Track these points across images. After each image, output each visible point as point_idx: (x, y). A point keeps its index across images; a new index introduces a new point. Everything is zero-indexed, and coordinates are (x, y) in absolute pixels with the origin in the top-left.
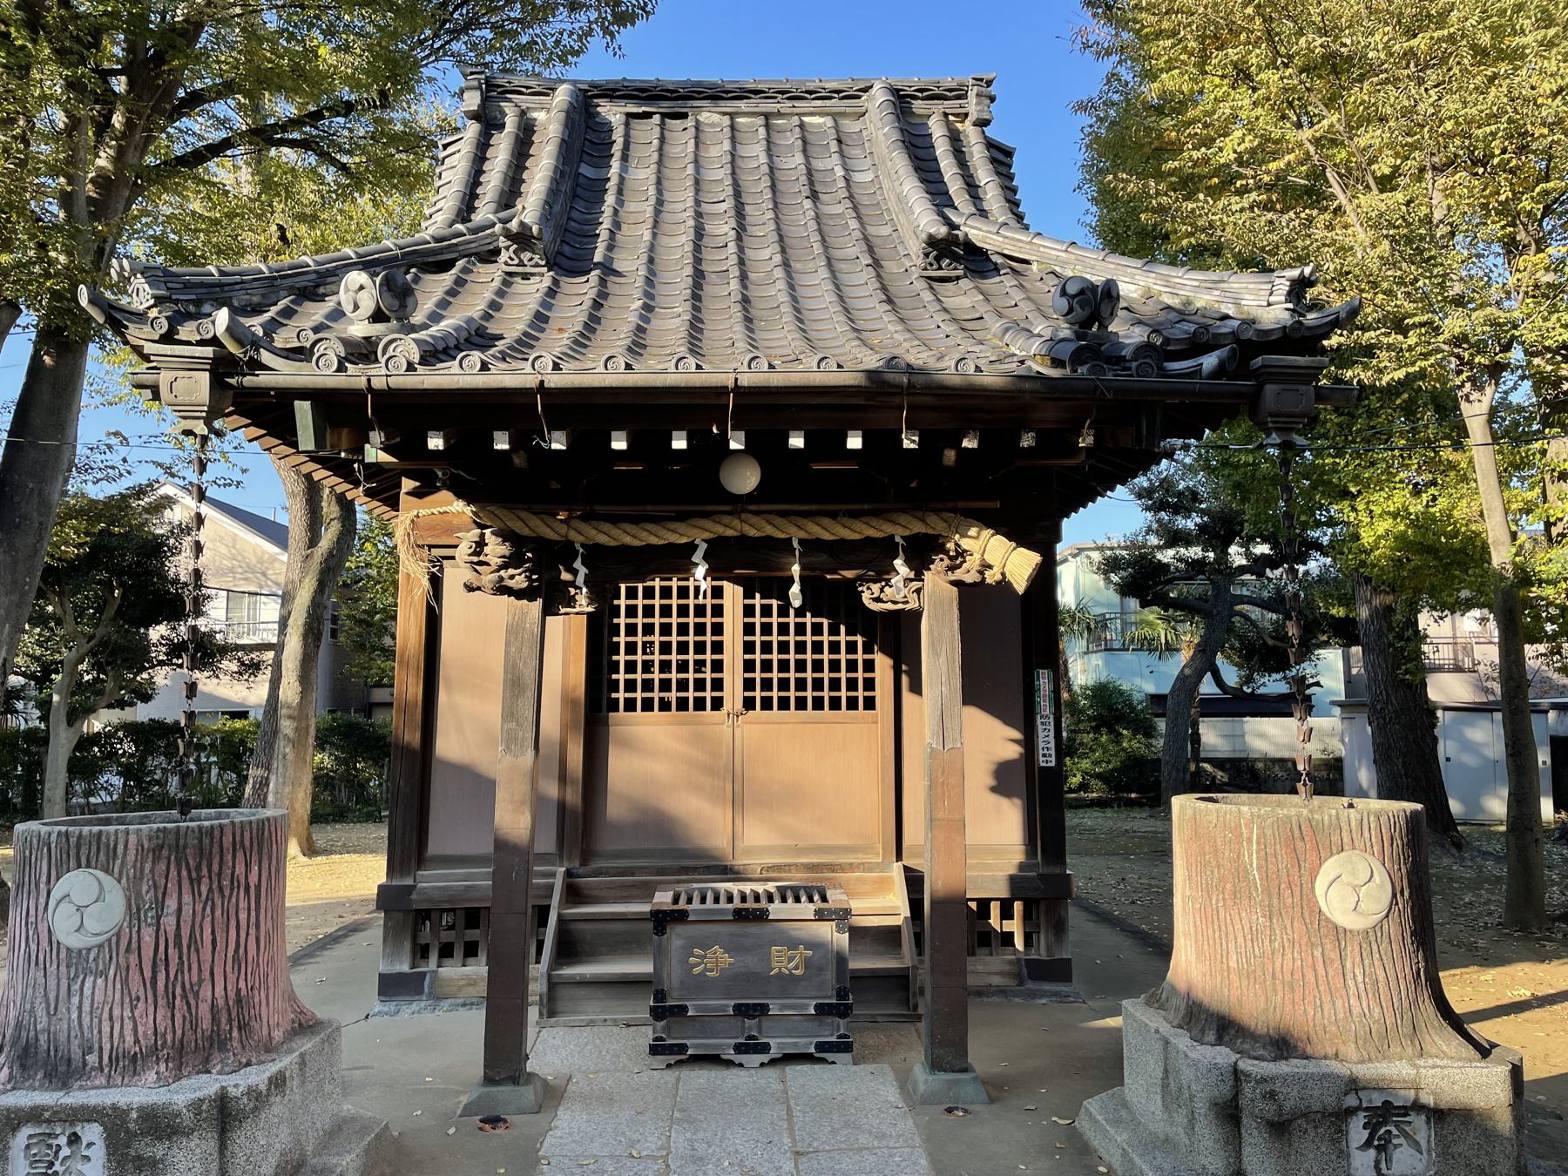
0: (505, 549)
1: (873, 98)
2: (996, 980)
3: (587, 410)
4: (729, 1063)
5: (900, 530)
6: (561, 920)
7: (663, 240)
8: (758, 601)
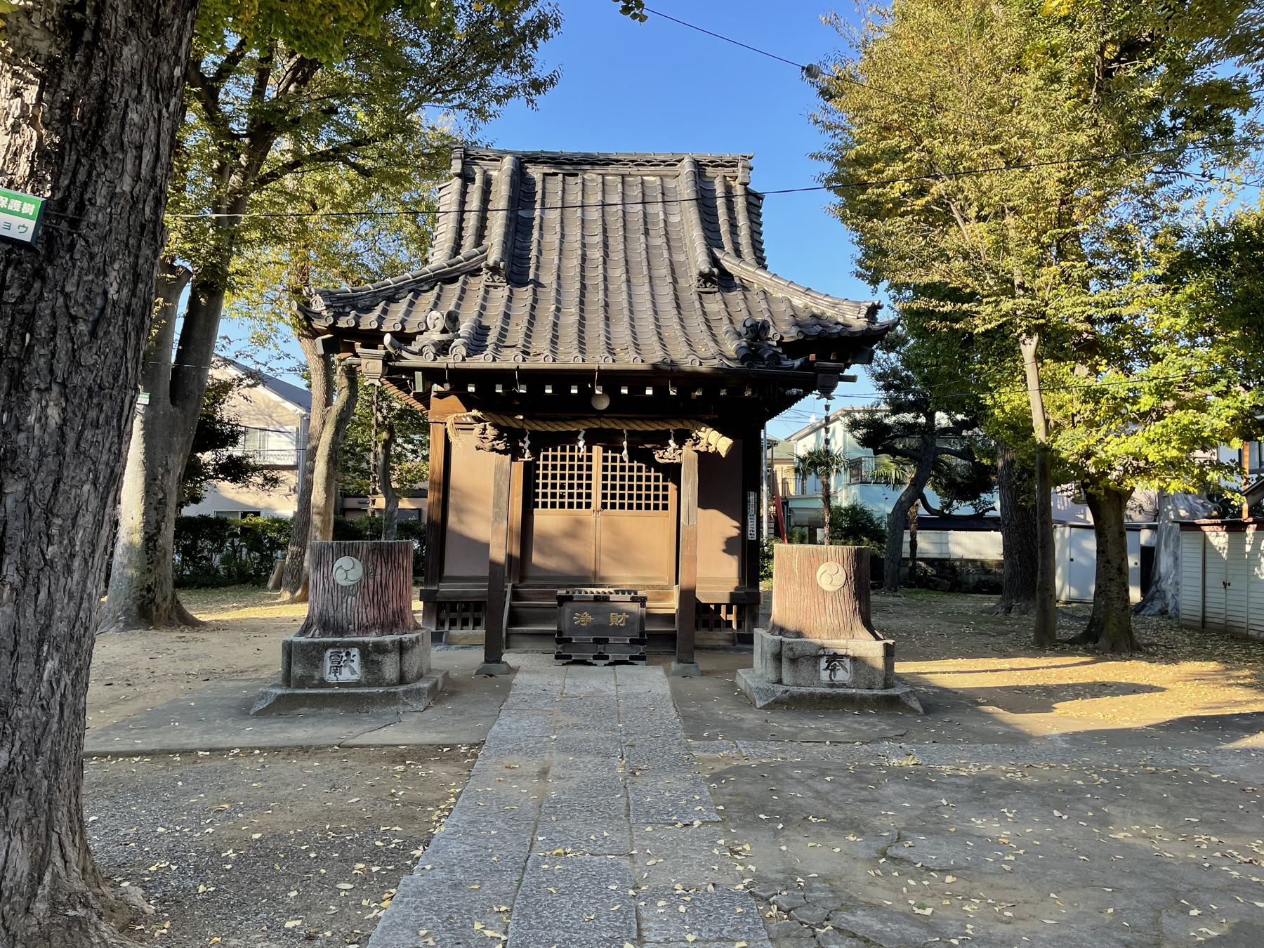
0: (495, 432)
1: (683, 167)
2: (722, 643)
3: (535, 378)
4: (591, 664)
5: (672, 428)
6: (511, 606)
7: (565, 262)
8: (610, 454)
